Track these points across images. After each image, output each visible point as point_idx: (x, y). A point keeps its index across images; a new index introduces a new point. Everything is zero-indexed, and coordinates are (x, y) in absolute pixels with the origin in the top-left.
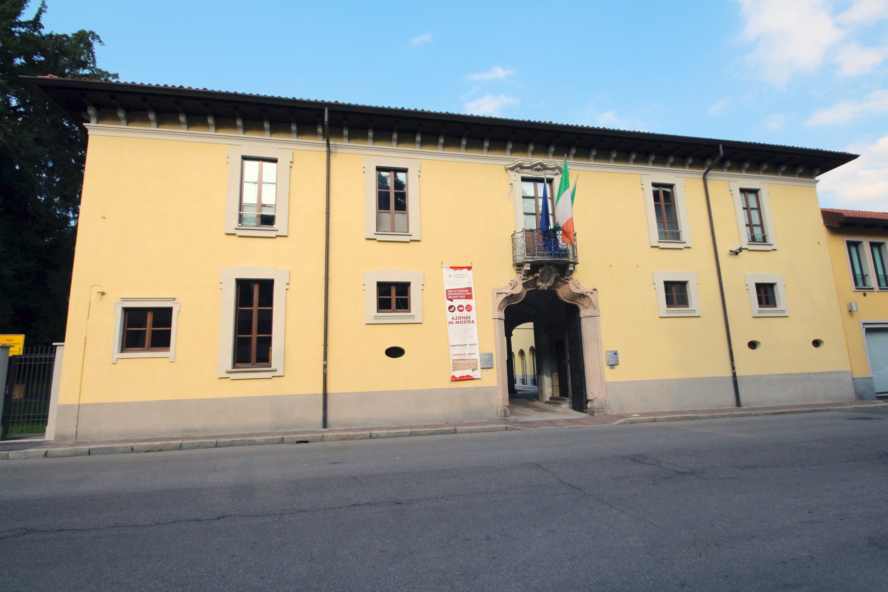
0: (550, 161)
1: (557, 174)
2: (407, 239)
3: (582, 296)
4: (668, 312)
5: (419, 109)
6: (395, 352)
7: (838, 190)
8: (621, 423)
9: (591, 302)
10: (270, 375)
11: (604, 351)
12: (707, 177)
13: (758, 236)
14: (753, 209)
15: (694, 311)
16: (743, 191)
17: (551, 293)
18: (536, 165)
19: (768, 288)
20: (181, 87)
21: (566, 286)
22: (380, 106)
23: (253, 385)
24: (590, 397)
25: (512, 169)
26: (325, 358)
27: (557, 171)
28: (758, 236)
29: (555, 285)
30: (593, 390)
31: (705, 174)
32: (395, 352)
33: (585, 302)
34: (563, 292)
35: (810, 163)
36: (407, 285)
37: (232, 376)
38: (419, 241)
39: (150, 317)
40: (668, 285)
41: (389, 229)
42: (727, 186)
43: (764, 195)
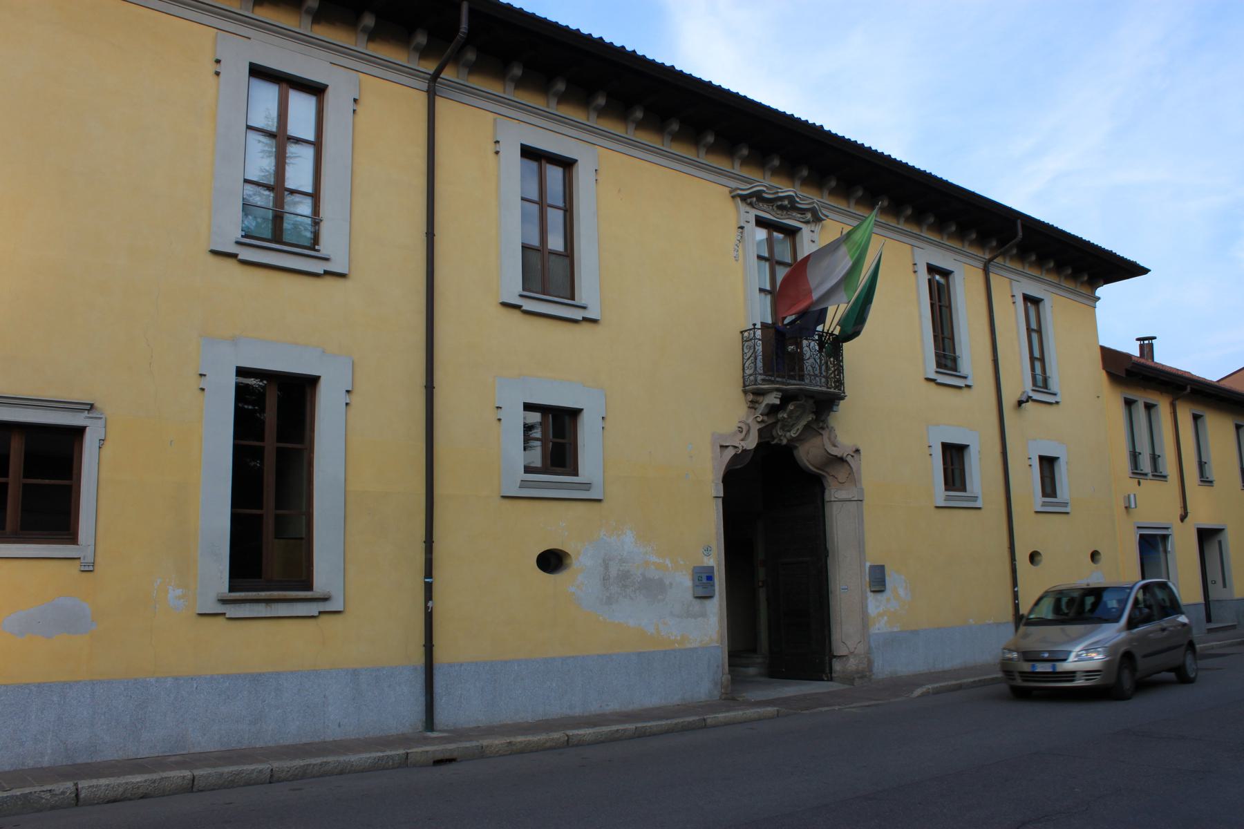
0: (807, 197)
1: (807, 222)
2: (318, 267)
3: (842, 460)
4: (1044, 504)
5: (629, 48)
6: (551, 561)
7: (1119, 316)
8: (923, 695)
9: (851, 472)
10: (313, 609)
11: (868, 564)
12: (991, 268)
13: (549, 275)
14: (298, 141)
15: (587, 486)
16: (528, 153)
17: (787, 452)
18: (782, 198)
19: (567, 419)
20: (623, 47)
21: (816, 441)
22: (563, 22)
23: (272, 641)
24: (839, 648)
25: (744, 198)
26: (429, 572)
27: (809, 216)
28: (549, 275)
29: (800, 439)
30: (846, 636)
31: (991, 260)
32: (551, 561)
33: (842, 474)
34: (808, 454)
35: (1092, 266)
36: (575, 413)
37: (232, 611)
38: (342, 276)
39: (16, 450)
40: (946, 447)
41: (268, 235)
42: (1012, 285)
43: (583, 176)
